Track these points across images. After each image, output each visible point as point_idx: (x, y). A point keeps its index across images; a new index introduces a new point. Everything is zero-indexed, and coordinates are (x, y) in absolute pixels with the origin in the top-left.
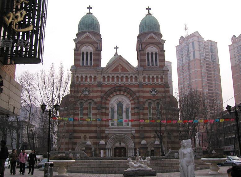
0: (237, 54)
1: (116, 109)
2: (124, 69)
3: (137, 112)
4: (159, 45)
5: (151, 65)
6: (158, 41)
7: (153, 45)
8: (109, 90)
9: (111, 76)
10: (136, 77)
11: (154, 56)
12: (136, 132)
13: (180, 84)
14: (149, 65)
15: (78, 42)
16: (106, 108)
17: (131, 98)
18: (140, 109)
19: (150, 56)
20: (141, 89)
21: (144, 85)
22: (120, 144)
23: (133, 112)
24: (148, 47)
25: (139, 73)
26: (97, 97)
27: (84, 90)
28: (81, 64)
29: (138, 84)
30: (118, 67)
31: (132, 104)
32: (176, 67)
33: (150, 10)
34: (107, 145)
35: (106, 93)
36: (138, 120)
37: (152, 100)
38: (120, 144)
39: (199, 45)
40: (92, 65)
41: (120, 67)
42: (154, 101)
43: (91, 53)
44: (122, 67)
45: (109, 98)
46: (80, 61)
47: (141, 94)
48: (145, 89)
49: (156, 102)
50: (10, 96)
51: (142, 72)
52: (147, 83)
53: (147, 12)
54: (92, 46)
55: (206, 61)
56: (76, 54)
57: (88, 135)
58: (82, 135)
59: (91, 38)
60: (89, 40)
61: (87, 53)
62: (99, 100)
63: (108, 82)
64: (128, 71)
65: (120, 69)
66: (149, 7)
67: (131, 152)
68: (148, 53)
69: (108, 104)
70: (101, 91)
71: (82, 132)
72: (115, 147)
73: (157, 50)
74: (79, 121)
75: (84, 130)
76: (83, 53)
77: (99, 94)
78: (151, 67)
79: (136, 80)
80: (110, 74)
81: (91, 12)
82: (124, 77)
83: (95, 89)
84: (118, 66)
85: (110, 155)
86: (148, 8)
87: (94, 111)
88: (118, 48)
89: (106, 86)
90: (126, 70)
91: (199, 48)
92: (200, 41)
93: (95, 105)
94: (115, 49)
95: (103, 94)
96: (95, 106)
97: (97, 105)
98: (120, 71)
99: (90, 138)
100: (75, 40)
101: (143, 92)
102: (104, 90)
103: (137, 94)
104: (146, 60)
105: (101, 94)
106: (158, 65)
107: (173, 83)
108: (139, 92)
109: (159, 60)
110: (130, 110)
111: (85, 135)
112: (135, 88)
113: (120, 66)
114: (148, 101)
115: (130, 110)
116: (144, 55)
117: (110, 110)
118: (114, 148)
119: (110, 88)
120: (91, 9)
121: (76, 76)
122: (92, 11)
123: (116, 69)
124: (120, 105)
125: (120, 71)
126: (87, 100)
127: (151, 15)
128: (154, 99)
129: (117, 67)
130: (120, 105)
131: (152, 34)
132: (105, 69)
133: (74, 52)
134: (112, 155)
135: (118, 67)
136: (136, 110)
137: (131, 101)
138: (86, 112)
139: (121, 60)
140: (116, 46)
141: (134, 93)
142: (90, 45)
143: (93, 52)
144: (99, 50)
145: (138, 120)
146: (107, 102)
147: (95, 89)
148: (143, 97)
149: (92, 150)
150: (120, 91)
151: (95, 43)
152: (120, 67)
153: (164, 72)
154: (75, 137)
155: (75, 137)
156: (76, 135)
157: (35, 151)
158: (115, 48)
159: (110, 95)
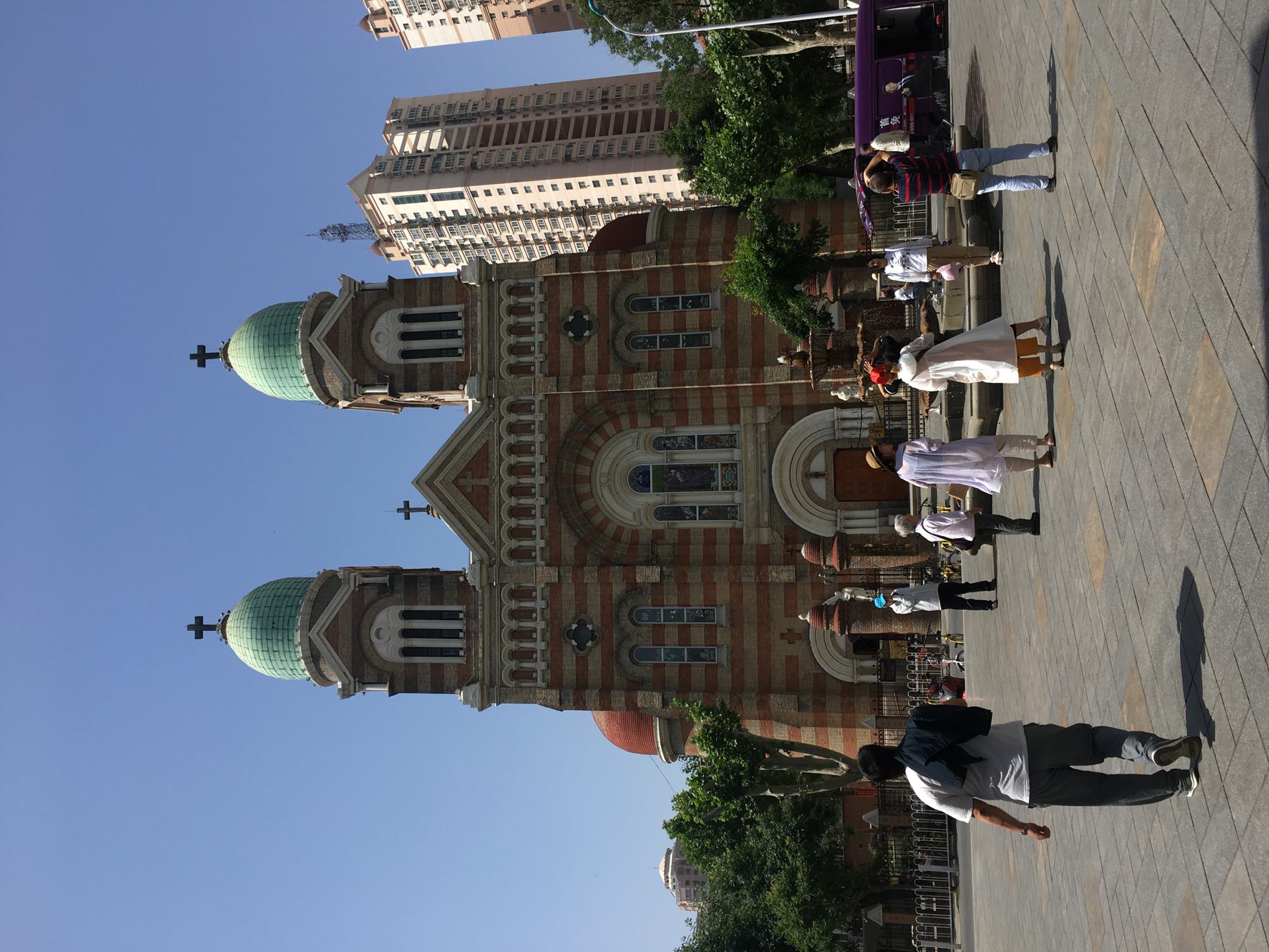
0: (441, 14)
2: (480, 463)
4: (367, 302)
6: (345, 311)
8: (571, 526)
12: (764, 405)
13: (495, 138)
16: (652, 541)
17: (609, 428)
22: (817, 475)
23: (670, 418)
26: (605, 584)
27: (574, 643)
30: (469, 490)
31: (634, 425)
34: (808, 417)
37: (616, 332)
38: (817, 475)
45: (588, 505)
49: (623, 313)
55: (474, 145)
56: (411, 688)
60: (346, 628)
65: (475, 482)
66: (193, 357)
67: (855, 424)
69: (635, 533)
71: (765, 647)
84: (462, 489)
85: (872, 522)
86: (196, 361)
88: (407, 503)
100: (392, 692)
104: (432, 364)
110: (659, 432)
111: (782, 636)
112: (563, 408)
113: (462, 482)
115: (659, 432)
117: (660, 525)
118: (837, 504)
120: (205, 623)
123: (481, 501)
124: (640, 479)
125: (485, 481)
130: (640, 479)
131: (313, 340)
132: (481, 550)
134: (869, 509)
135: (469, 490)
137: (619, 430)
141: (583, 411)
146: (625, 537)
157: (815, 224)
158: (407, 517)
159: (592, 438)
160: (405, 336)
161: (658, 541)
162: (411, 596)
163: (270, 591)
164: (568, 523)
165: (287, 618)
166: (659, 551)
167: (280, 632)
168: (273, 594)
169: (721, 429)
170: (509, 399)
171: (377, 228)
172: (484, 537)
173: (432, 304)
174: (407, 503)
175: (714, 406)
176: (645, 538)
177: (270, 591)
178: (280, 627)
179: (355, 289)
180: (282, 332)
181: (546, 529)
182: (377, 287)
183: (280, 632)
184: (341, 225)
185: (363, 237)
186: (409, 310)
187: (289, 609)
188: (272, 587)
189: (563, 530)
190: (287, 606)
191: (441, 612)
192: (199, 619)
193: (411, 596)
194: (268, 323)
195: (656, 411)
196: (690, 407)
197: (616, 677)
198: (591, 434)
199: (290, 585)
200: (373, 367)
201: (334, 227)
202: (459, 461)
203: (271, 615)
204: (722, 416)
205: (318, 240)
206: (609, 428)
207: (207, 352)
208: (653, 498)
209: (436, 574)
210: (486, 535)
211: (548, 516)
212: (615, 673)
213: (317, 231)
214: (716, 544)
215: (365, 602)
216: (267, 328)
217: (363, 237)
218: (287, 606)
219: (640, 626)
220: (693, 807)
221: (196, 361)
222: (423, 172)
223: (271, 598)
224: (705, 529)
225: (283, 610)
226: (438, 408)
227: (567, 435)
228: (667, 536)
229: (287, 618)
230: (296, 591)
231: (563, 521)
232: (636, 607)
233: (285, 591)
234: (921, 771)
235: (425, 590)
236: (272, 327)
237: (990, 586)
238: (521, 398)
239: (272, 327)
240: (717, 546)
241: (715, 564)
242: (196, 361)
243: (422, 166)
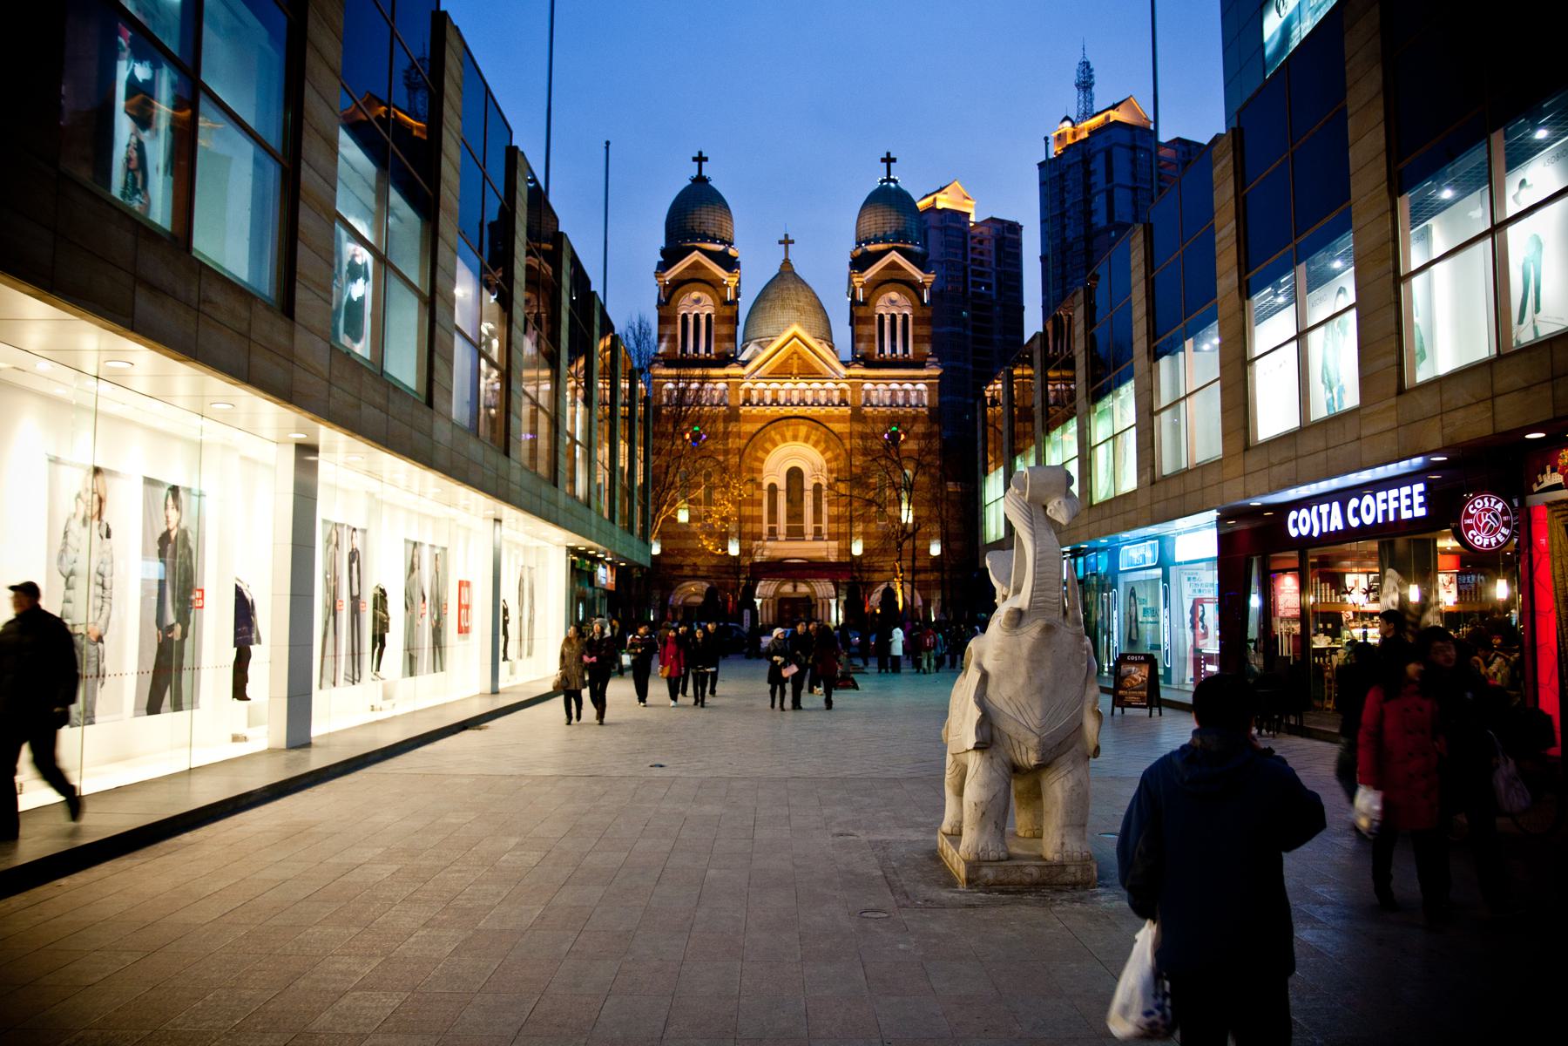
32: (1038, 252)
33: (892, 164)
39: (1133, 162)
50: (253, 337)
54: (714, 293)
72: (780, 596)
86: (885, 156)
88: (792, 242)
91: (1134, 176)
92: (1139, 143)
94: (783, 246)
107: (1025, 313)
113: (795, 356)
116: (868, 320)
117: (765, 486)
124: (795, 475)
130: (795, 475)
140: (786, 236)
158: (780, 242)
169: (824, 526)
173: (914, 336)
174: (792, 242)
184: (1093, 84)
185: (1081, 106)
192: (706, 159)
205: (1079, 59)
208: (782, 484)
213: (1089, 58)
234: (1161, 952)
237: (703, 706)
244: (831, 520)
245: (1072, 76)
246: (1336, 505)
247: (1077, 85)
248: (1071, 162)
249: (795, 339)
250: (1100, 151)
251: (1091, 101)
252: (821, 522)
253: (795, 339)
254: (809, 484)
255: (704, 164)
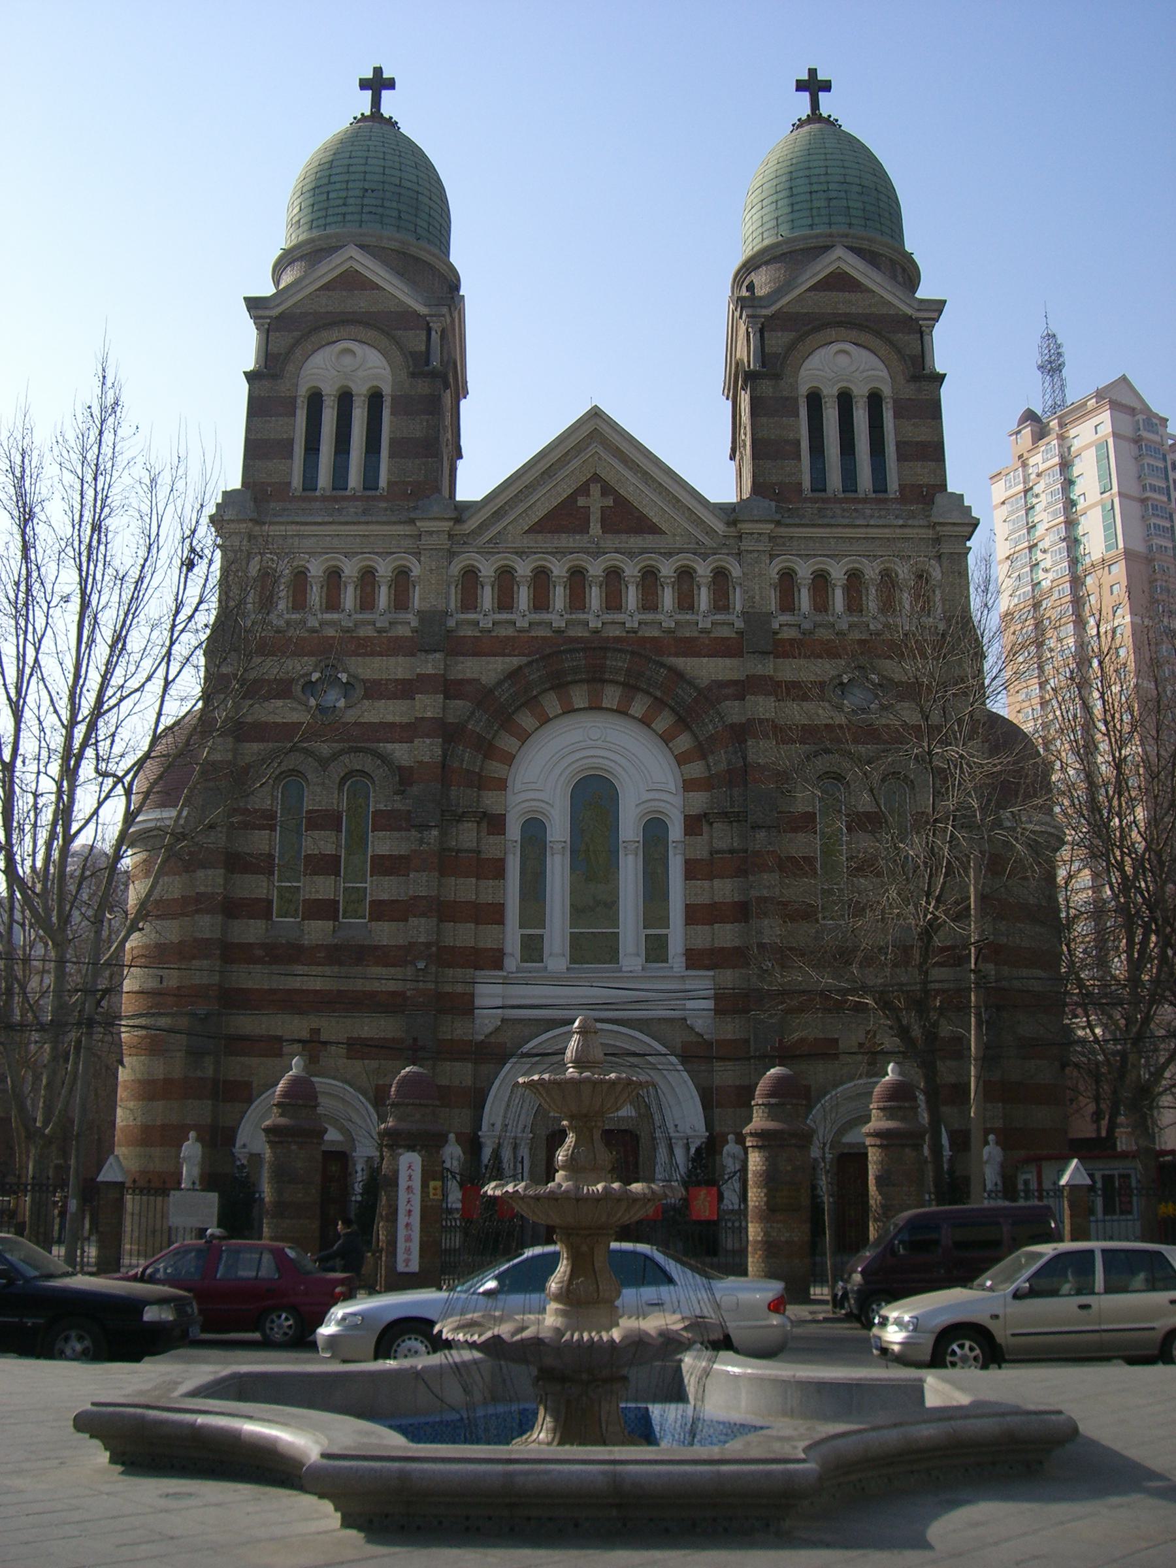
1: (559, 830)
3: (731, 852)
4: (900, 338)
5: (834, 480)
7: (853, 334)
8: (513, 675)
9: (524, 569)
10: (720, 576)
11: (861, 417)
14: (819, 483)
15: (281, 317)
16: (484, 813)
17: (684, 742)
18: (756, 827)
19: (831, 416)
20: (766, 667)
21: (788, 634)
24: (384, 354)
25: (746, 545)
26: (409, 731)
27: (315, 676)
28: (297, 481)
29: (740, 633)
33: (822, 96)
35: (483, 696)
36: (742, 912)
40: (383, 482)
41: (595, 502)
42: (324, 763)
43: (375, 399)
44: (609, 502)
46: (290, 456)
47: (763, 707)
48: (789, 670)
49: (337, 770)
51: (771, 538)
52: (807, 625)
53: (363, 102)
56: (257, 409)
57: (333, 1028)
58: (296, 1026)
59: (377, 287)
60: (360, 303)
61: (345, 399)
62: (426, 750)
63: (537, 617)
64: (654, 530)
66: (813, 72)
68: (815, 400)
69: (502, 785)
70: (450, 688)
71: (292, 1002)
73: (884, 373)
74: (268, 915)
75: (373, 995)
76: (315, 400)
77: (428, 706)
78: (865, 500)
79: (400, 601)
80: (520, 553)
81: (386, 111)
82: (628, 572)
83: (398, 668)
84: (584, 490)
87: (382, 844)
89: (480, 647)
90: (642, 525)
93: (402, 792)
95: (460, 707)
96: (399, 804)
97: (415, 790)
98: (595, 528)
99: (357, 1048)
100: (249, 376)
101: (795, 691)
102: (469, 676)
103: (735, 712)
104: (798, 443)
105: (444, 709)
106: (893, 485)
108: (744, 688)
109: (898, 445)
110: (676, 832)
113: (595, 490)
114: (345, 759)
115: (676, 832)
117: (514, 831)
119: (516, 661)
121: (254, 569)
122: (390, 104)
125: (595, 528)
126: (335, 756)
127: (386, 128)
128: (325, 749)
129: (572, 498)
131: (839, 252)
133: (244, 387)
135: (581, 501)
136: (723, 837)
138: (329, 849)
139: (606, 443)
142: (371, 334)
143: (387, 390)
144: (434, 374)
145: (742, 912)
147: (398, 668)
148: (780, 732)
149: (815, 1152)
150: (596, 678)
151: (407, 318)
152: (595, 502)
153: (937, 540)
154: (240, 1044)
155: (240, 1044)
156: (248, 1024)
159: (666, 713)
160: (845, 400)
161: (484, 825)
162: (403, 405)
163: (428, 186)
164: (520, 667)
165: (380, 210)
166: (466, 825)
167: (359, 201)
168: (420, 189)
169: (677, 936)
170: (736, 571)
171: (1060, 418)
172: (499, 527)
175: (716, 926)
176: (490, 801)
177: (428, 186)
178: (366, 201)
179: (925, 319)
180: (851, 204)
181: (510, 632)
182: (927, 358)
183: (359, 201)
184: (1062, 365)
185: (1047, 397)
186: (890, 405)
187: (395, 214)
188: (433, 190)
189: (507, 659)
190: (400, 212)
191: (378, 452)
192: (390, 84)
193: (403, 405)
194: (865, 183)
195: (711, 824)
196: (717, 883)
197: (255, 747)
198: (672, 709)
199: (438, 217)
200: (791, 347)
201: (1060, 355)
202: (631, 488)
203: (387, 187)
204: (704, 937)
205: (1041, 331)
206: (684, 742)
207: (820, 94)
209: (446, 453)
210: (505, 528)
211: (533, 634)
212: (262, 746)
213: (1054, 329)
214: (477, 923)
215: (399, 333)
216: (857, 181)
217: (1047, 397)
218: (400, 212)
219: (340, 790)
220: (697, 1175)
221: (806, 77)
222: (1144, 488)
223: (416, 187)
224: (502, 905)
225: (394, 205)
226: (731, 459)
227: (671, 669)
228: (492, 839)
229: (380, 210)
230: (425, 225)
231: (524, 660)
232: (373, 783)
233: (427, 209)
235: (416, 428)
236: (858, 189)
238: (738, 590)
239: (858, 189)
240: (472, 926)
241: (441, 921)
242: (806, 77)
243: (1154, 489)
244: (693, 915)
245: (1034, 357)
246: (401, 1267)
247: (1040, 367)
248: (1042, 467)
249: (595, 448)
250: (1087, 447)
251: (1062, 387)
252: (665, 922)
253: (595, 448)
254: (629, 828)
255: (386, 94)
